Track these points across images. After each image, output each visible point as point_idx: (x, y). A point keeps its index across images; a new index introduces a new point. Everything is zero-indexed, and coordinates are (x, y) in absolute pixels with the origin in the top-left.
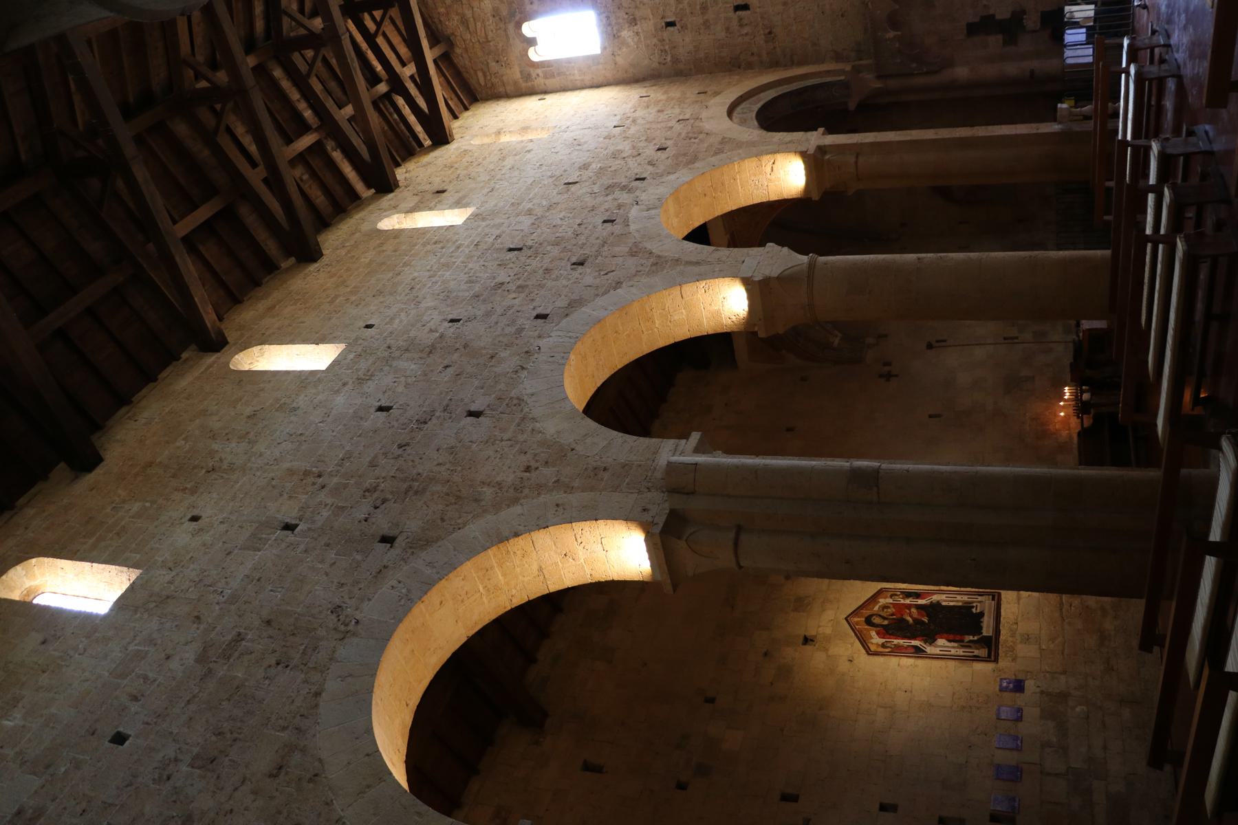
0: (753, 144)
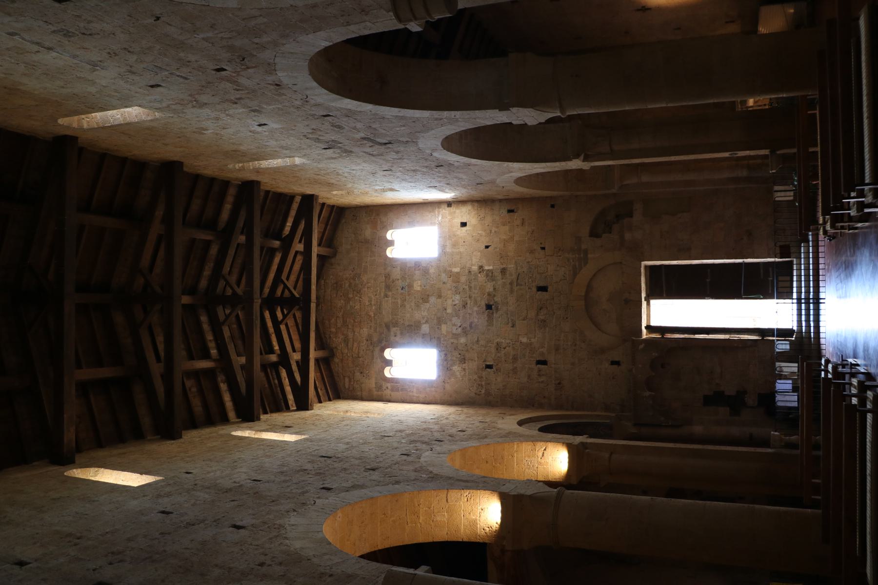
0: (532, 436)
